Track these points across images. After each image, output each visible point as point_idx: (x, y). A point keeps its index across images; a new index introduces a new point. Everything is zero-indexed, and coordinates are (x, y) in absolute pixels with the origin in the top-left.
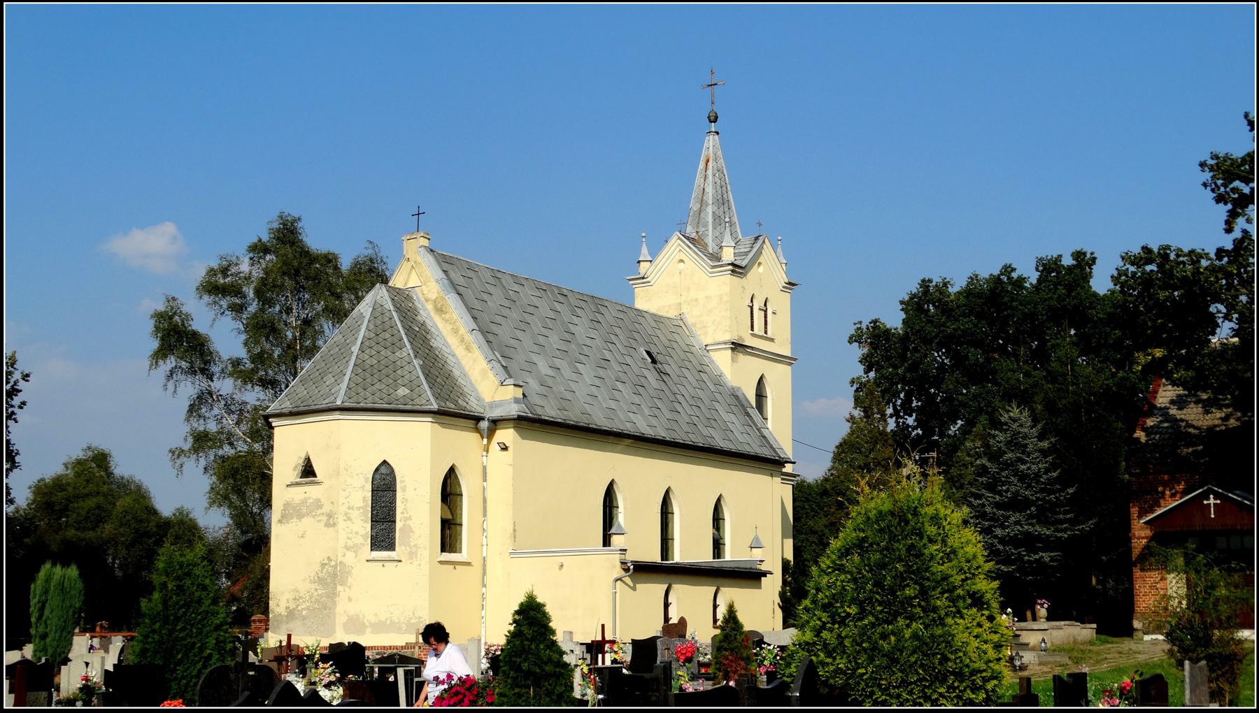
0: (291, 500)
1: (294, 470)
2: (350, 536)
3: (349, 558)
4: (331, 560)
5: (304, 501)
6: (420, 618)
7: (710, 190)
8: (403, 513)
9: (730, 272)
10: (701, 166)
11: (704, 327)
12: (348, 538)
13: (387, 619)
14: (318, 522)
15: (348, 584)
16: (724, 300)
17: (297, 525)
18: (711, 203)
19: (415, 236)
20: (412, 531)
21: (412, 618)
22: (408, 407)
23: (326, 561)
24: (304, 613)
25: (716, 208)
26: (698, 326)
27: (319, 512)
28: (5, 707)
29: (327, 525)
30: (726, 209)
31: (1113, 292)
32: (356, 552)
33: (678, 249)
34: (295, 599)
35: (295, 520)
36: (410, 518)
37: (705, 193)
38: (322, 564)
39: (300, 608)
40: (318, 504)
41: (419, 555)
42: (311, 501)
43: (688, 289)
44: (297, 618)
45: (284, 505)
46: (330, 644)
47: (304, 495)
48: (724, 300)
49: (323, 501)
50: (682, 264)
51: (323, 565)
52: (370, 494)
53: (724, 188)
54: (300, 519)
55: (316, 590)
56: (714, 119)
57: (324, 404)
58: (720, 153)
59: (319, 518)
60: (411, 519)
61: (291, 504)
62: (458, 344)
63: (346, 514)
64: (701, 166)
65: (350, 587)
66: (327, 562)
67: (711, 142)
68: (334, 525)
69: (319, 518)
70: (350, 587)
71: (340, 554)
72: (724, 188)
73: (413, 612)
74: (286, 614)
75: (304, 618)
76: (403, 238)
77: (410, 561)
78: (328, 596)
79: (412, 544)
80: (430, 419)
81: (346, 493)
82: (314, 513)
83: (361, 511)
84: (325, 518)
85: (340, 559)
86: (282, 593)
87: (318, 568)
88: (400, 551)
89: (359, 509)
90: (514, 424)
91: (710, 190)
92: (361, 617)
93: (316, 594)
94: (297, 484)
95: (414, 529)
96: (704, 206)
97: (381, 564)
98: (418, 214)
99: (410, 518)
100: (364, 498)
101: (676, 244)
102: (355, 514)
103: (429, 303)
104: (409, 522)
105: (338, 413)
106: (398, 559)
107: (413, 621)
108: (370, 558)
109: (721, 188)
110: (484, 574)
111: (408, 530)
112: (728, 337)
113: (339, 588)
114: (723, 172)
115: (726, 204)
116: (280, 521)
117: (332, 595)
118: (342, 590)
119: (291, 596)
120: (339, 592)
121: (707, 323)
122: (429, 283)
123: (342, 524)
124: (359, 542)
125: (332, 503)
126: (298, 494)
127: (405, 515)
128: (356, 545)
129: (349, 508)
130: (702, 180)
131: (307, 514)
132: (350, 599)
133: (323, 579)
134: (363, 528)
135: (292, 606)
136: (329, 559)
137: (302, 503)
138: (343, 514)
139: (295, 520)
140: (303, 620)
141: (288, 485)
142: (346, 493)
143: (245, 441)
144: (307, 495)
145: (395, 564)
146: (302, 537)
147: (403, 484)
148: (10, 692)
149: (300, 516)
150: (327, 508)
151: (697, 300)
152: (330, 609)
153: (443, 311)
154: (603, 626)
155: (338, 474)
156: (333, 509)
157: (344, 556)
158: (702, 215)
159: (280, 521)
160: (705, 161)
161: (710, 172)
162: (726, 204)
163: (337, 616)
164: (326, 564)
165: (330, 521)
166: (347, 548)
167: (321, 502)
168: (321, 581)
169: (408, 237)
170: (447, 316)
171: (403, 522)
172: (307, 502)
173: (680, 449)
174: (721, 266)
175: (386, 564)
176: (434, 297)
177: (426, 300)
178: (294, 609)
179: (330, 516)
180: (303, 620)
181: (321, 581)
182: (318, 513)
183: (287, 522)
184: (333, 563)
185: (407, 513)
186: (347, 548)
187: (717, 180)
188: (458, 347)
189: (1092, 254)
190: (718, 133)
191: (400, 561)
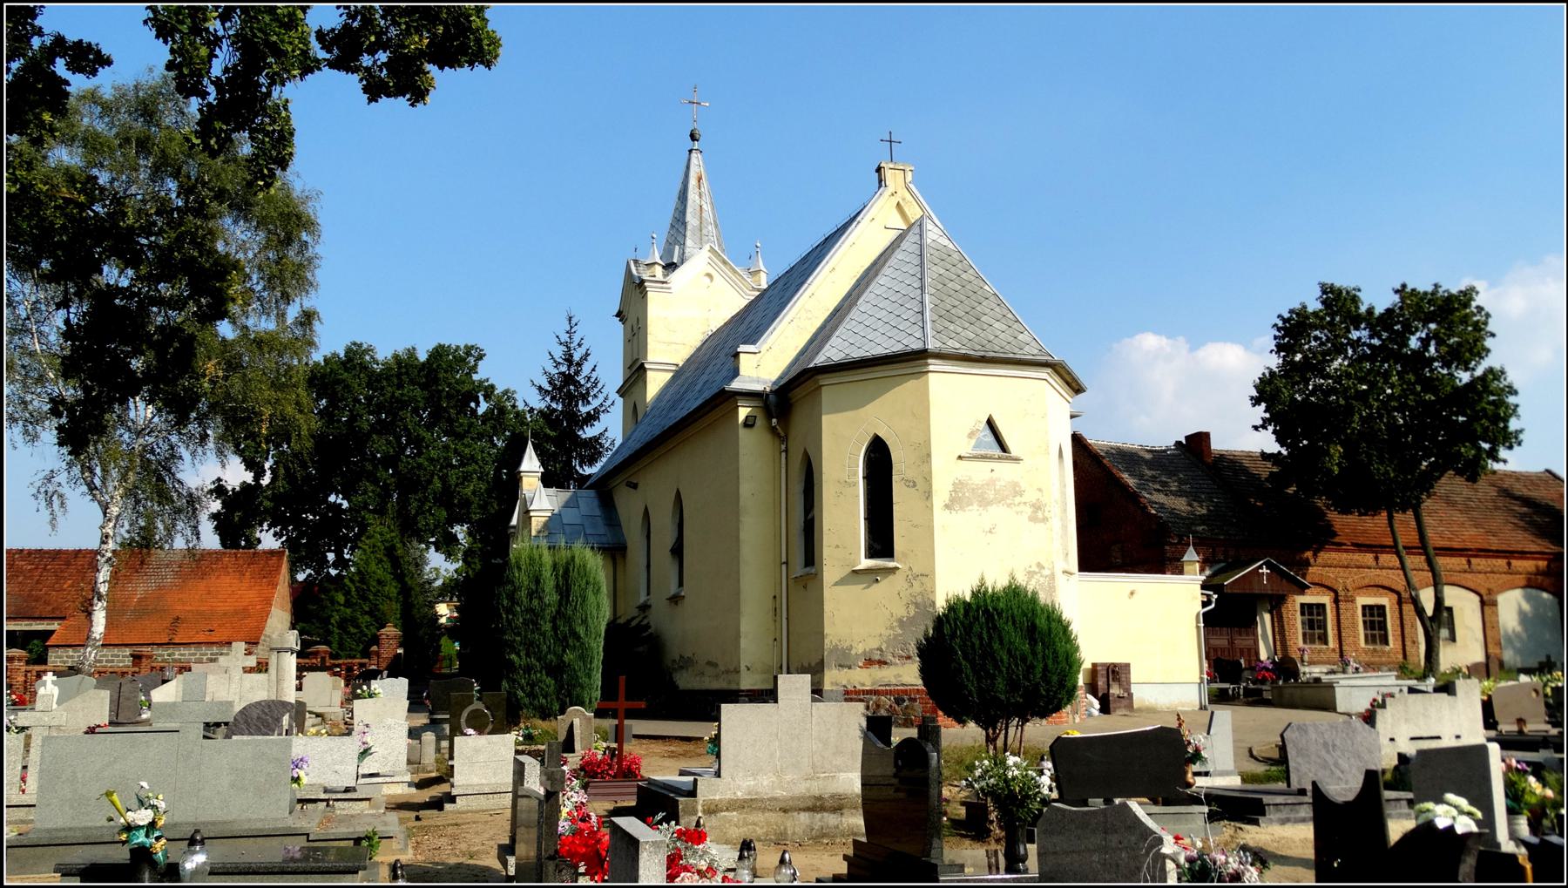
5: (991, 483)
23: (1035, 568)
27: (1018, 499)
28: (1565, 5)
29: (1033, 519)
31: (1275, 432)
35: (975, 507)
38: (1029, 572)
54: (986, 506)
59: (1018, 509)
61: (967, 484)
66: (1037, 570)
68: (1045, 520)
82: (1008, 501)
84: (1029, 510)
110: (1421, 738)
116: (947, 507)
125: (1040, 490)
126: (979, 472)
130: (697, 197)
136: (1039, 565)
137: (988, 485)
139: (975, 507)
143: (1552, 822)
146: (990, 532)
149: (985, 503)
150: (1031, 496)
154: (1439, 738)
156: (1042, 499)
159: (947, 507)
164: (1035, 573)
167: (1019, 487)
173: (884, 367)
179: (1037, 507)
183: (962, 508)
184: (1046, 572)
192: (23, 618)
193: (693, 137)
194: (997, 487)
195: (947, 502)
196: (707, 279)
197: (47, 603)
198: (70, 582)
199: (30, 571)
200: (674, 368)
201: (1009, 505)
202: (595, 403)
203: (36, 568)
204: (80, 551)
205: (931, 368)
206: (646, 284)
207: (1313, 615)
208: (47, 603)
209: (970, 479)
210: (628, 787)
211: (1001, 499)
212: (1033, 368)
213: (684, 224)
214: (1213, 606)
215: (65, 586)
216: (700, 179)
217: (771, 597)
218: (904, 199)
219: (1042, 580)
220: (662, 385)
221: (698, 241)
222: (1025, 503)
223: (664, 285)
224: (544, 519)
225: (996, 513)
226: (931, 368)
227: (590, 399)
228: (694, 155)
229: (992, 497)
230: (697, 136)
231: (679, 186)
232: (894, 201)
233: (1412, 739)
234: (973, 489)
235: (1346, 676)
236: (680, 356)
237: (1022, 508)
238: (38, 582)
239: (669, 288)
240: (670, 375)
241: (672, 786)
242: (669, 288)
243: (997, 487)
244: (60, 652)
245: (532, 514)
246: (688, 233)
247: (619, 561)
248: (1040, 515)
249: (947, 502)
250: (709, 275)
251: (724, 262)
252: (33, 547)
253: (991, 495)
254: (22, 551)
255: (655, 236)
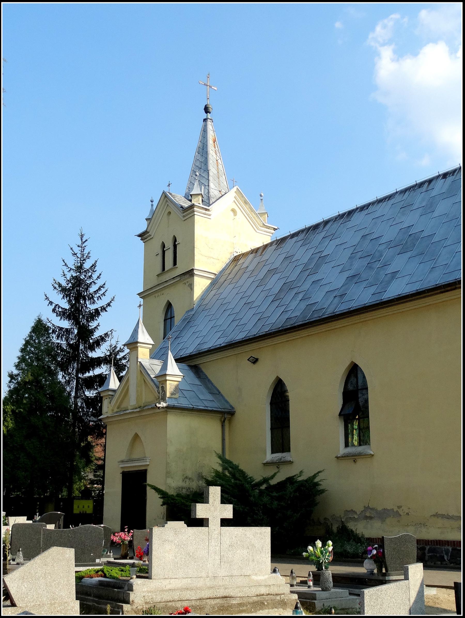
28: (2, 3)
193: (207, 110)
196: (232, 214)
200: (213, 276)
202: (99, 304)
206: (195, 209)
207: (455, 546)
210: (305, 586)
213: (207, 171)
217: (276, 468)
220: (204, 288)
221: (217, 185)
223: (207, 212)
224: (176, 383)
227: (96, 299)
228: (209, 122)
230: (210, 110)
231: (195, 144)
236: (217, 268)
239: (210, 215)
240: (209, 282)
242: (210, 215)
245: (168, 378)
246: (211, 178)
247: (227, 423)
250: (233, 211)
251: (246, 202)
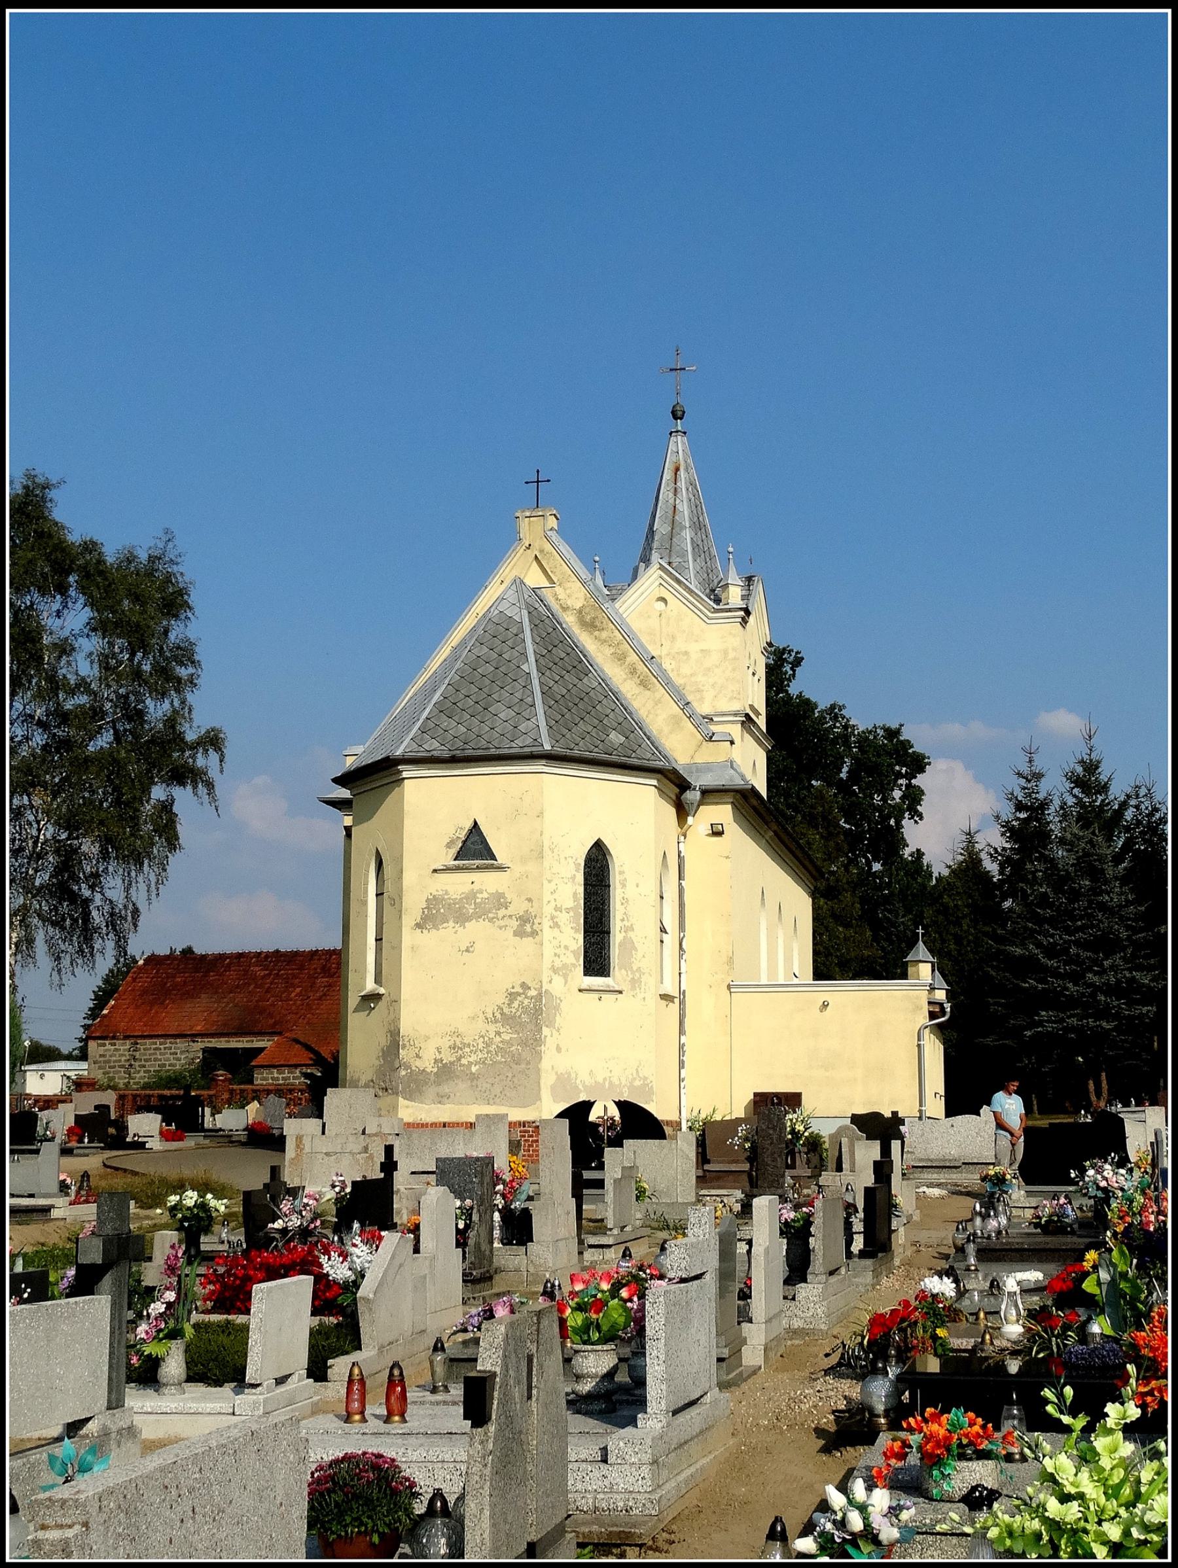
0: (441, 893)
1: (449, 845)
2: (557, 951)
3: (556, 986)
4: (529, 988)
5: (471, 896)
6: (645, 1078)
7: (684, 508)
8: (623, 920)
9: (740, 620)
10: (668, 475)
11: (699, 691)
12: (555, 955)
13: (605, 1079)
14: (501, 928)
15: (556, 1025)
16: (730, 657)
17: (456, 933)
18: (688, 526)
19: (540, 513)
20: (636, 950)
21: (635, 1079)
22: (635, 762)
24: (474, 1069)
25: (693, 534)
26: (688, 688)
29: (520, 933)
30: (704, 537)
32: (565, 976)
33: (657, 583)
34: (453, 1047)
35: (451, 924)
36: (631, 928)
37: (677, 512)
39: (464, 1061)
40: (500, 901)
41: (643, 984)
42: (485, 895)
43: (673, 638)
44: (458, 1077)
45: (428, 900)
46: (756, 1095)
47: (469, 887)
48: (730, 657)
49: (509, 896)
50: (663, 604)
51: (512, 996)
52: (581, 890)
53: (699, 508)
55: (498, 1033)
56: (677, 415)
57: (520, 744)
58: (690, 461)
59: (502, 923)
60: (633, 930)
61: (443, 899)
62: (625, 676)
63: (552, 918)
64: (668, 475)
65: (558, 1030)
67: (679, 446)
68: (534, 933)
69: (502, 923)
70: (558, 1030)
71: (545, 980)
72: (699, 508)
73: (637, 1071)
74: (435, 1070)
75: (473, 1077)
76: (517, 514)
77: (632, 993)
78: (524, 1043)
79: (635, 969)
80: (655, 782)
81: (552, 886)
82: (491, 915)
83: (572, 914)
84: (515, 924)
85: (545, 986)
86: (427, 1038)
87: (501, 999)
88: (618, 976)
89: (568, 910)
90: (734, 798)
91: (684, 508)
92: (573, 1075)
93: (498, 1039)
94: (447, 869)
95: (636, 945)
96: (677, 529)
97: (596, 996)
98: (538, 482)
99: (631, 928)
100: (575, 894)
101: (655, 576)
102: (563, 918)
103: (569, 613)
104: (630, 934)
105: (543, 762)
106: (617, 989)
107: (637, 1083)
108: (584, 987)
109: (696, 507)
111: (629, 946)
112: (736, 706)
113: (546, 1031)
114: (696, 487)
115: (703, 530)
116: (418, 926)
117: (533, 1042)
118: (549, 1034)
119: (446, 1043)
120: (546, 1037)
121: (703, 686)
122: (569, 585)
123: (547, 933)
124: (568, 962)
125: (530, 900)
126: (458, 884)
127: (626, 923)
128: (565, 966)
129: (557, 909)
130: (671, 495)
131: (477, 916)
132: (559, 1049)
133: (513, 1017)
134: (574, 939)
135: (448, 1057)
136: (524, 986)
138: (549, 917)
139: (451, 924)
140: (472, 1080)
141: (435, 871)
142: (552, 886)
144: (476, 887)
145: (613, 996)
146: (467, 950)
147: (622, 877)
148: (1050, 1124)
149: (462, 918)
150: (518, 906)
151: (686, 653)
152: (528, 1063)
153: (596, 627)
155: (541, 856)
156: (531, 910)
157: (550, 982)
158: (674, 539)
159: (418, 926)
160: (673, 468)
161: (682, 484)
162: (703, 530)
163: (543, 1075)
164: (519, 994)
165: (526, 926)
166: (555, 970)
168: (507, 1019)
169: (528, 514)
170: (604, 635)
171: (624, 934)
172: (475, 898)
174: (730, 610)
175: (604, 996)
176: (578, 605)
177: (562, 608)
178: (452, 1063)
179: (525, 919)
180: (472, 1080)
181: (507, 1019)
182: (500, 916)
183: (436, 927)
184: (533, 993)
185: (628, 920)
186: (555, 970)
187: (691, 496)
188: (625, 680)
189: (798, 653)
190: (685, 433)
191: (621, 992)
192: (235, 1035)
193: (677, 415)
194: (478, 901)
195: (418, 920)
197: (271, 1015)
198: (298, 990)
199: (264, 977)
201: (491, 920)
203: (270, 974)
204: (317, 951)
205: (405, 774)
208: (271, 1015)
209: (447, 893)
211: (481, 913)
212: (531, 762)
214: (946, 1018)
215: (293, 995)
216: (677, 469)
218: (542, 551)
219: (526, 1002)
222: (510, 916)
225: (476, 929)
226: (405, 774)
229: (471, 911)
232: (531, 554)
233: (413, 1173)
234: (449, 905)
235: (1129, 1109)
237: (506, 921)
238: (267, 991)
241: (1022, 1260)
243: (478, 901)
244: (266, 1073)
248: (528, 928)
249: (418, 920)
252: (267, 945)
253: (471, 909)
254: (260, 953)
255: (597, 559)
